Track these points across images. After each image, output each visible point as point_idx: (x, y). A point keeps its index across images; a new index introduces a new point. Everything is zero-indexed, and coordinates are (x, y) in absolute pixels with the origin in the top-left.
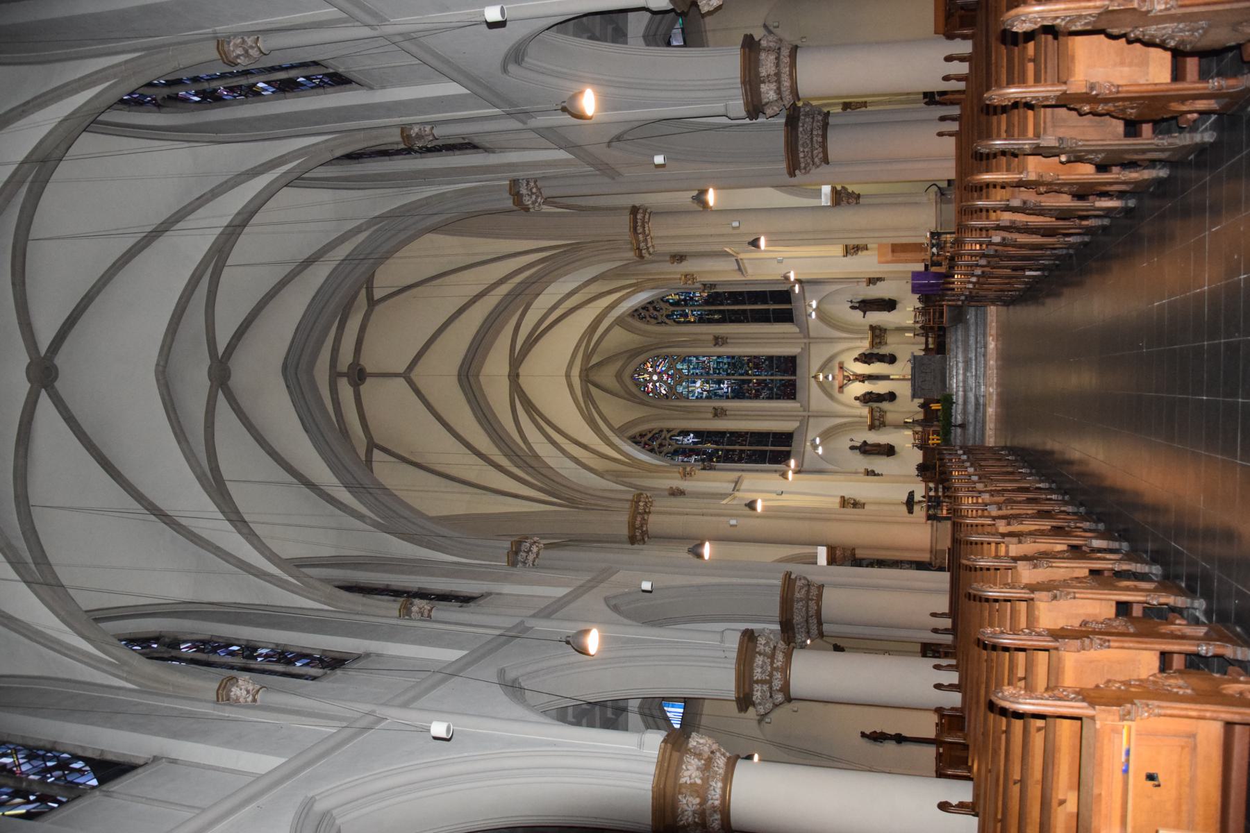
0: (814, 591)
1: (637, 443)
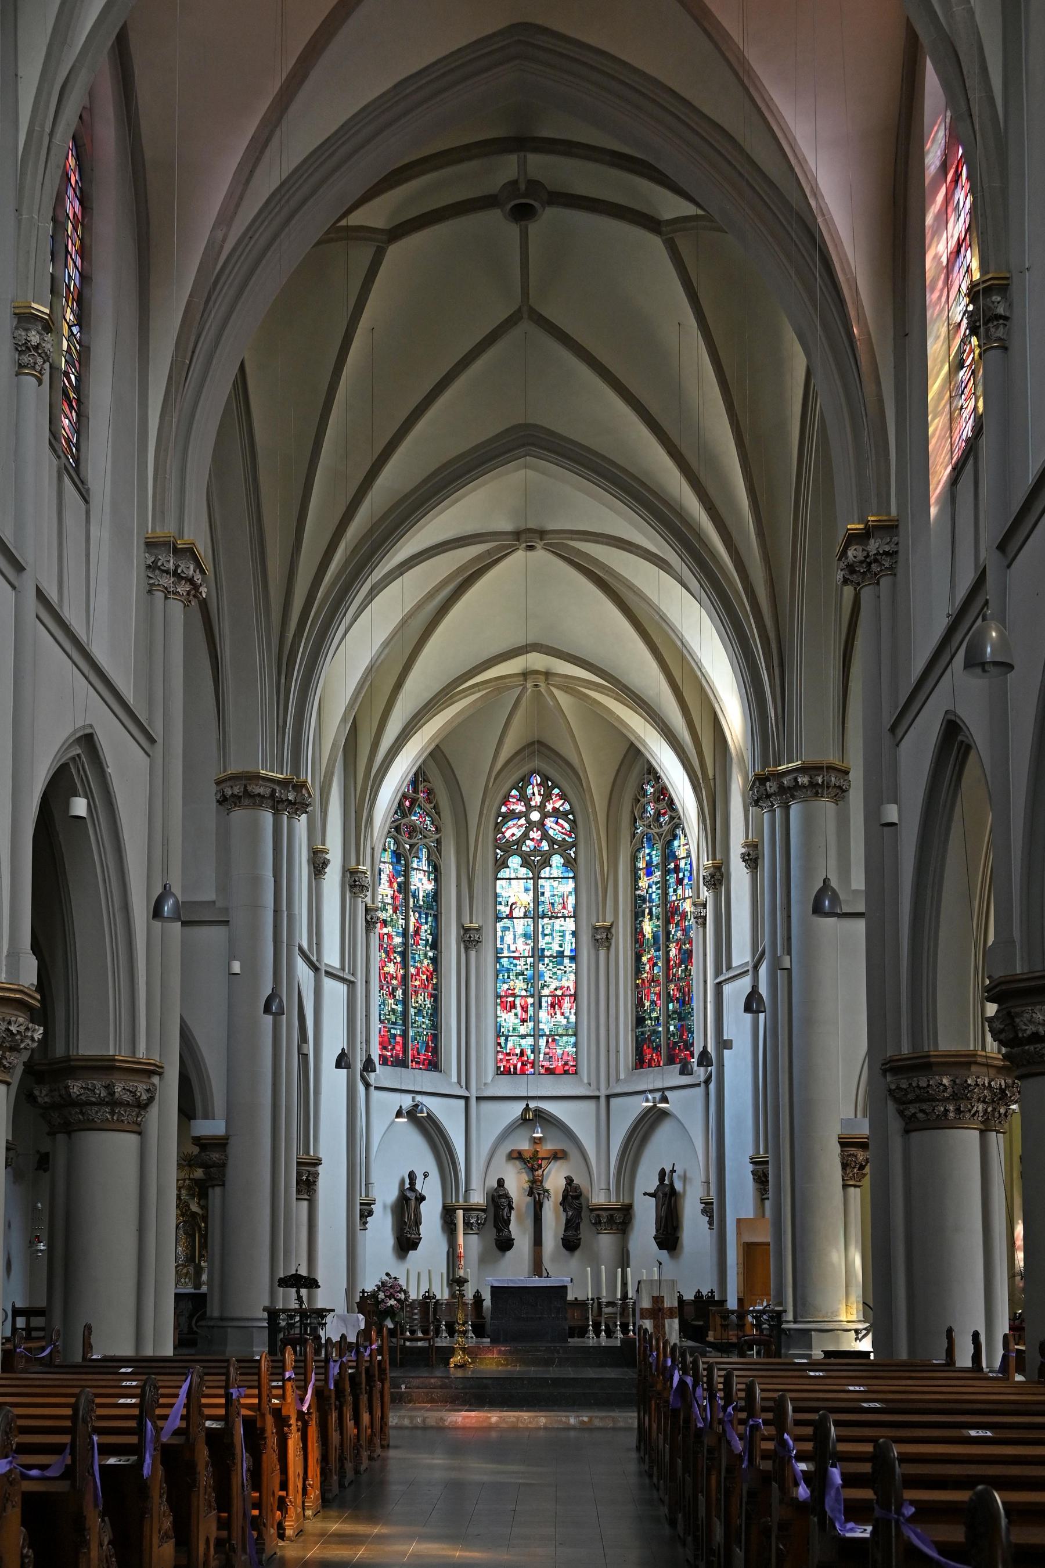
0: (128, 1115)
1: (415, 782)
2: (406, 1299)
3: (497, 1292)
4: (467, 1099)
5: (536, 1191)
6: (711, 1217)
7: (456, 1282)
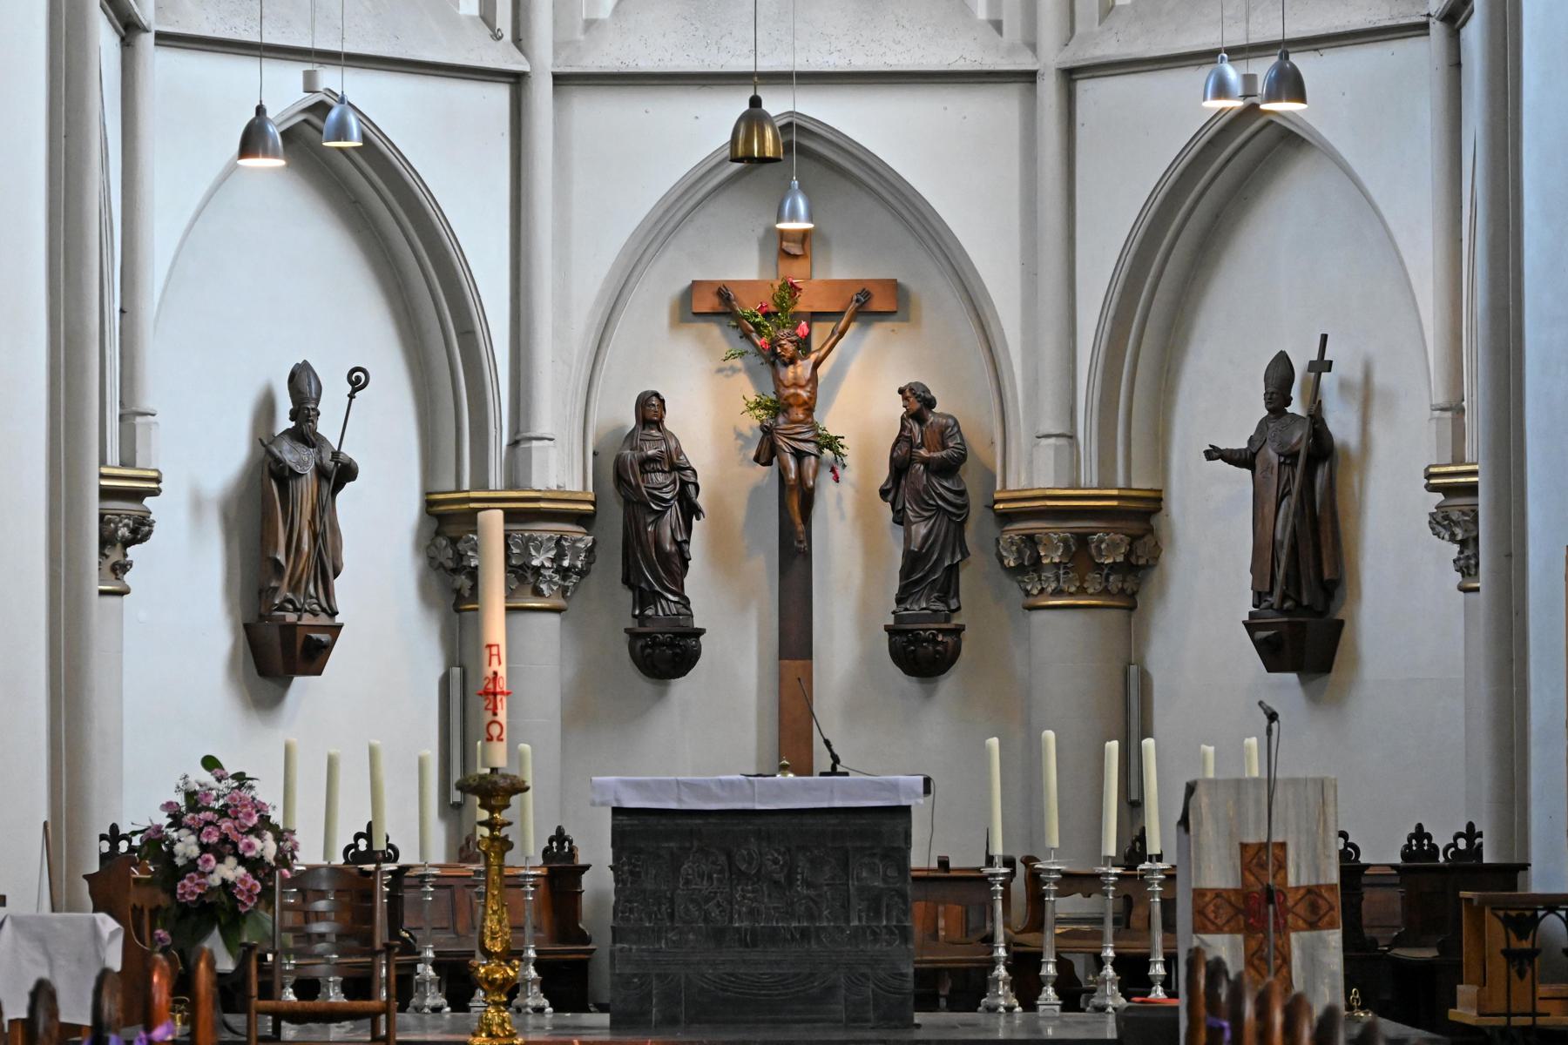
2: (284, 859)
3: (636, 830)
4: (517, 81)
5: (788, 444)
6: (1468, 544)
7: (478, 793)
